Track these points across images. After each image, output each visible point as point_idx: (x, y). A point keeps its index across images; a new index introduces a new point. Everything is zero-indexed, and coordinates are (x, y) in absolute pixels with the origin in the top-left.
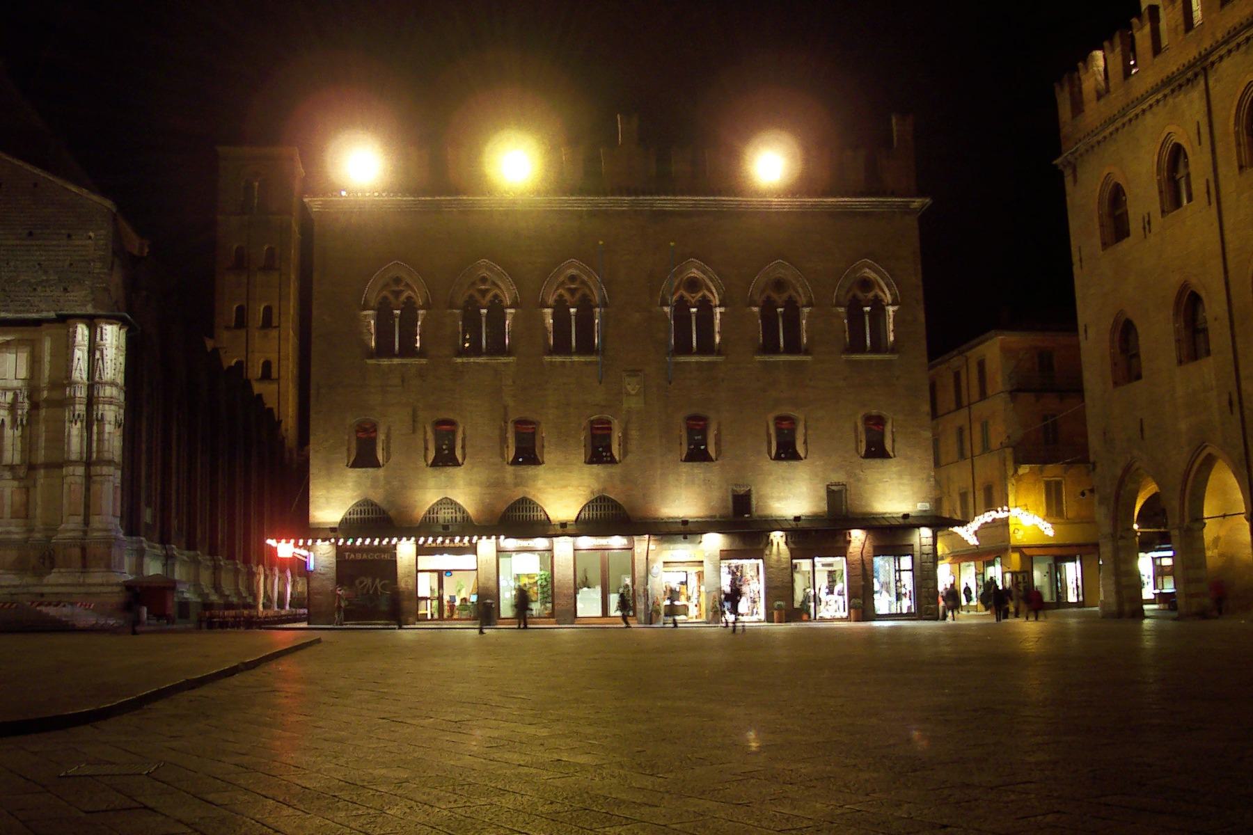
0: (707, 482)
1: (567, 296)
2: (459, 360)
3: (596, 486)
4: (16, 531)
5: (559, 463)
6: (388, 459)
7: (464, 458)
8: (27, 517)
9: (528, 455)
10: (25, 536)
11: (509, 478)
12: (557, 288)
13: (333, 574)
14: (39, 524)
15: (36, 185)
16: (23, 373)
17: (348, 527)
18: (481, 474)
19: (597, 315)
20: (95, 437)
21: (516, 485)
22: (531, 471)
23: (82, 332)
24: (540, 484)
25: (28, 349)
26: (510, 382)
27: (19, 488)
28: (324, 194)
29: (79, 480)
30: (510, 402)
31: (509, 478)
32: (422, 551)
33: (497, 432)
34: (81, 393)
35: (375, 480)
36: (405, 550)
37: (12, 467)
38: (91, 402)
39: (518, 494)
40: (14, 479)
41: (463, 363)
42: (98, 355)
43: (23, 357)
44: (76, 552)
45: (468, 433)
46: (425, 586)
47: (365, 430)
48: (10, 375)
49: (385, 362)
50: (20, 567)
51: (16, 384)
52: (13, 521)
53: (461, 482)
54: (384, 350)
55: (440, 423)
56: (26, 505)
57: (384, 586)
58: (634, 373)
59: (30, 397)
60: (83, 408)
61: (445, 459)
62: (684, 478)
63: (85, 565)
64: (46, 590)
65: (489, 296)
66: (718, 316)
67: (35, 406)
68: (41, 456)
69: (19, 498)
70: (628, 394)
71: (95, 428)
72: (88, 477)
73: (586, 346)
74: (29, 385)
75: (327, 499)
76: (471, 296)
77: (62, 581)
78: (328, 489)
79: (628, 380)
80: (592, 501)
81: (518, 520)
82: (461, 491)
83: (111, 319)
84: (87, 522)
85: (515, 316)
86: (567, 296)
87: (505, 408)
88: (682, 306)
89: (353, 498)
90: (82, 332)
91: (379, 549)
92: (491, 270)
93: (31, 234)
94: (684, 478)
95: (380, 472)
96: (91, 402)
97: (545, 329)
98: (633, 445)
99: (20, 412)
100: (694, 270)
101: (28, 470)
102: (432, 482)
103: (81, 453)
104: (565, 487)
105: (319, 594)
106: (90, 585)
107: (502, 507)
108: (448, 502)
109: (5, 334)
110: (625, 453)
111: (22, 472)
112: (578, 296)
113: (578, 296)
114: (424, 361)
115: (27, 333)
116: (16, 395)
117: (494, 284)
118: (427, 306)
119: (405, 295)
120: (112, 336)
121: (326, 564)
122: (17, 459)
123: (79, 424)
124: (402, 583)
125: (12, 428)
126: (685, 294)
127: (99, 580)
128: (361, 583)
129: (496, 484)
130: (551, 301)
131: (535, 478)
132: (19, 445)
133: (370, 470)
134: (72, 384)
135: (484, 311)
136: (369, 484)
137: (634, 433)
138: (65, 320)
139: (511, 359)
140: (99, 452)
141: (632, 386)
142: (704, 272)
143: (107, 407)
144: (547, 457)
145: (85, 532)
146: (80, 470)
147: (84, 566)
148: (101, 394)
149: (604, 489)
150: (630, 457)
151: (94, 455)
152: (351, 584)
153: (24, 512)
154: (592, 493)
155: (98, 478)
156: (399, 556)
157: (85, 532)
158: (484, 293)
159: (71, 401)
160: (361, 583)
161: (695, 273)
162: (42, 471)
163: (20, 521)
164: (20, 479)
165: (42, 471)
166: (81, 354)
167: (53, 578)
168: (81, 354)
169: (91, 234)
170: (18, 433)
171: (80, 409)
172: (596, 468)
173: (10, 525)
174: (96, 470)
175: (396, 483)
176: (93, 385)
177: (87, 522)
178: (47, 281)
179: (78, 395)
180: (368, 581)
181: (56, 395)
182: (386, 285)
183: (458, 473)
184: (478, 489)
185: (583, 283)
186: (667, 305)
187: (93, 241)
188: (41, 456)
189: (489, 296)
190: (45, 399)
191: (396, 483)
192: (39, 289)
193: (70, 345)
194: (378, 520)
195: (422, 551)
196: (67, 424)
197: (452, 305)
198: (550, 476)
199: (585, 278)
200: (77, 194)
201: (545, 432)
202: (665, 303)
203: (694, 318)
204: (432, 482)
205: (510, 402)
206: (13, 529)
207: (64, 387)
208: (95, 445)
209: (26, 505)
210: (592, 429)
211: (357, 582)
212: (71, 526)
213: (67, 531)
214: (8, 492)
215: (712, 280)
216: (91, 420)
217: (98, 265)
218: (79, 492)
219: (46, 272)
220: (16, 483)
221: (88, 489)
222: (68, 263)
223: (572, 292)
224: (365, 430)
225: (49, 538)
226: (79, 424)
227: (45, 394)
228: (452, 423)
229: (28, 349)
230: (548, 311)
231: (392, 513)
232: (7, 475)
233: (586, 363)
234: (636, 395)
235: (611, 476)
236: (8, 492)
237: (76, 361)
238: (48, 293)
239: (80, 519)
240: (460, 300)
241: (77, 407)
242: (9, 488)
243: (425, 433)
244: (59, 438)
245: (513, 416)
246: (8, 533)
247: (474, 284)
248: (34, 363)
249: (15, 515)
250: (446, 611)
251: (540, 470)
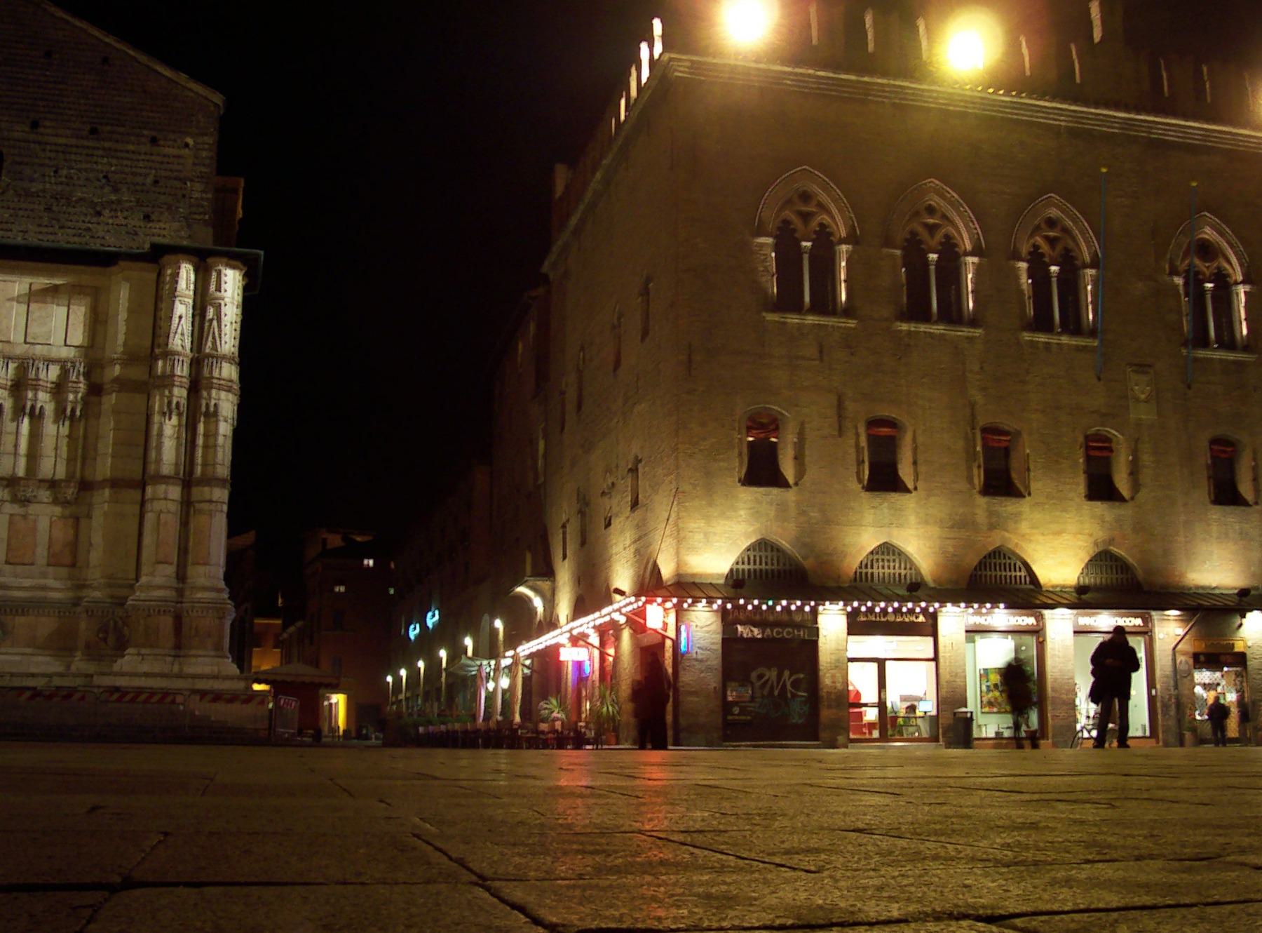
0: (1243, 535)
1: (1045, 248)
2: (904, 327)
3: (1101, 535)
4: (56, 587)
5: (1049, 497)
6: (800, 474)
7: (916, 479)
8: (73, 565)
9: (1001, 482)
10: (70, 594)
11: (981, 517)
12: (1032, 236)
13: (716, 661)
14: (95, 575)
15: (105, 60)
16: (78, 336)
17: (737, 583)
18: (940, 507)
19: (1088, 279)
20: (200, 441)
21: (992, 527)
22: (1009, 506)
23: (186, 274)
24: (1024, 527)
25: (89, 300)
26: (976, 368)
27: (63, 517)
28: (695, 52)
29: (174, 507)
30: (979, 398)
31: (981, 517)
32: (857, 626)
33: (961, 444)
34: (182, 370)
35: (782, 508)
36: (831, 620)
37: (53, 484)
38: (196, 385)
39: (994, 540)
40: (55, 501)
41: (909, 332)
42: (211, 313)
43: (80, 312)
44: (167, 622)
45: (920, 439)
46: (862, 681)
47: (762, 426)
48: (58, 338)
49: (793, 319)
50: (61, 644)
51: (65, 353)
52: (51, 569)
53: (912, 519)
54: (788, 301)
55: (873, 423)
56: (74, 545)
57: (796, 684)
58: (1142, 368)
59: (87, 375)
60: (184, 393)
61: (884, 480)
62: (1214, 529)
63: (180, 646)
64: (122, 682)
65: (939, 236)
66: (1243, 298)
67: (95, 390)
68: (104, 467)
69: (62, 534)
70: (1137, 400)
71: (201, 428)
72: (187, 503)
73: (1072, 324)
74: (86, 356)
75: (706, 535)
76: (913, 234)
77: (145, 668)
78: (708, 518)
79: (1135, 377)
80: (1087, 565)
81: (992, 579)
82: (908, 532)
83: (233, 259)
84: (181, 576)
85: (979, 270)
86: (1045, 248)
87: (972, 406)
88: (1194, 281)
89: (748, 536)
90: (186, 274)
91: (787, 619)
92: (942, 196)
93: (94, 131)
94: (1214, 528)
95: (790, 496)
96: (196, 385)
97: (1021, 292)
98: (1146, 476)
99: (71, 397)
100: (1208, 230)
101: (77, 490)
102: (869, 516)
103: (177, 464)
104: (1058, 533)
105: (695, 693)
106: (194, 677)
107: (972, 560)
108: (887, 550)
109: (52, 274)
110: (1136, 486)
111: (70, 492)
112: (1059, 248)
113: (1059, 248)
114: (852, 323)
115: (87, 275)
116: (65, 373)
117: (944, 217)
118: (851, 239)
119: (819, 219)
120: (231, 282)
121: (702, 643)
122: (61, 473)
123: (175, 420)
124: (827, 679)
125: (56, 421)
126: (1197, 262)
127: (207, 670)
128: (760, 677)
129: (962, 524)
130: (1025, 249)
131: (1017, 517)
132: (65, 449)
133: (775, 491)
134: (169, 355)
135: (933, 257)
136: (772, 514)
137: (1146, 459)
138: (158, 256)
139: (978, 332)
140: (205, 465)
141: (1140, 387)
142: (1221, 234)
143: (223, 394)
144: (1034, 486)
145: (180, 592)
146: (175, 492)
147: (178, 646)
148: (216, 374)
149: (1111, 541)
150: (1143, 495)
151: (198, 470)
152: (745, 681)
153: (70, 557)
154: (1096, 544)
155: (205, 506)
156: (822, 632)
157: (180, 592)
158: (932, 229)
159: (167, 381)
160: (760, 677)
161: (1208, 233)
162: (107, 492)
163: (63, 571)
164: (66, 503)
165: (107, 492)
166: (183, 309)
167: (129, 661)
168: (183, 309)
169: (190, 141)
170: (65, 430)
171: (180, 394)
172: (1100, 507)
173: (44, 575)
174: (197, 492)
175: (815, 514)
176: (200, 360)
177: (181, 576)
178: (119, 202)
179: (178, 372)
180: (772, 674)
181: (137, 373)
182: (789, 202)
183: (908, 503)
184: (935, 531)
185: (1066, 230)
186: (1178, 274)
187: (192, 151)
188: (104, 467)
189: (939, 236)
190: (119, 379)
191: (815, 514)
192: (106, 212)
193: (162, 297)
194: (787, 574)
195: (857, 626)
196: (156, 418)
197: (888, 242)
198: (1037, 516)
199: (1069, 223)
200: (170, 80)
201: (1028, 447)
202: (1174, 272)
203: (1209, 296)
204: (869, 516)
205: (979, 398)
206: (51, 582)
207: (153, 358)
208: (199, 452)
209: (74, 545)
210: (1088, 448)
211: (754, 675)
212: (158, 580)
213: (151, 587)
214: (43, 524)
215: (1231, 246)
216: (195, 413)
217: (199, 186)
218: (172, 522)
219: (116, 190)
220: (58, 510)
221: (185, 524)
222: (149, 180)
223: (1052, 242)
224: (762, 426)
225: (121, 602)
226: (175, 420)
227: (117, 370)
228: (891, 423)
229: (89, 300)
230: (1023, 265)
231: (808, 564)
232: (45, 495)
233: (1078, 349)
234: (1146, 401)
235: (1118, 520)
236: (43, 524)
237: (175, 320)
238: (121, 221)
239: (171, 570)
240: (901, 235)
241: (176, 391)
242: (45, 516)
243: (857, 435)
244: (145, 439)
245: (982, 421)
246: (44, 588)
247: (917, 214)
248: (97, 323)
249: (53, 561)
250: (889, 724)
251: (1024, 506)
